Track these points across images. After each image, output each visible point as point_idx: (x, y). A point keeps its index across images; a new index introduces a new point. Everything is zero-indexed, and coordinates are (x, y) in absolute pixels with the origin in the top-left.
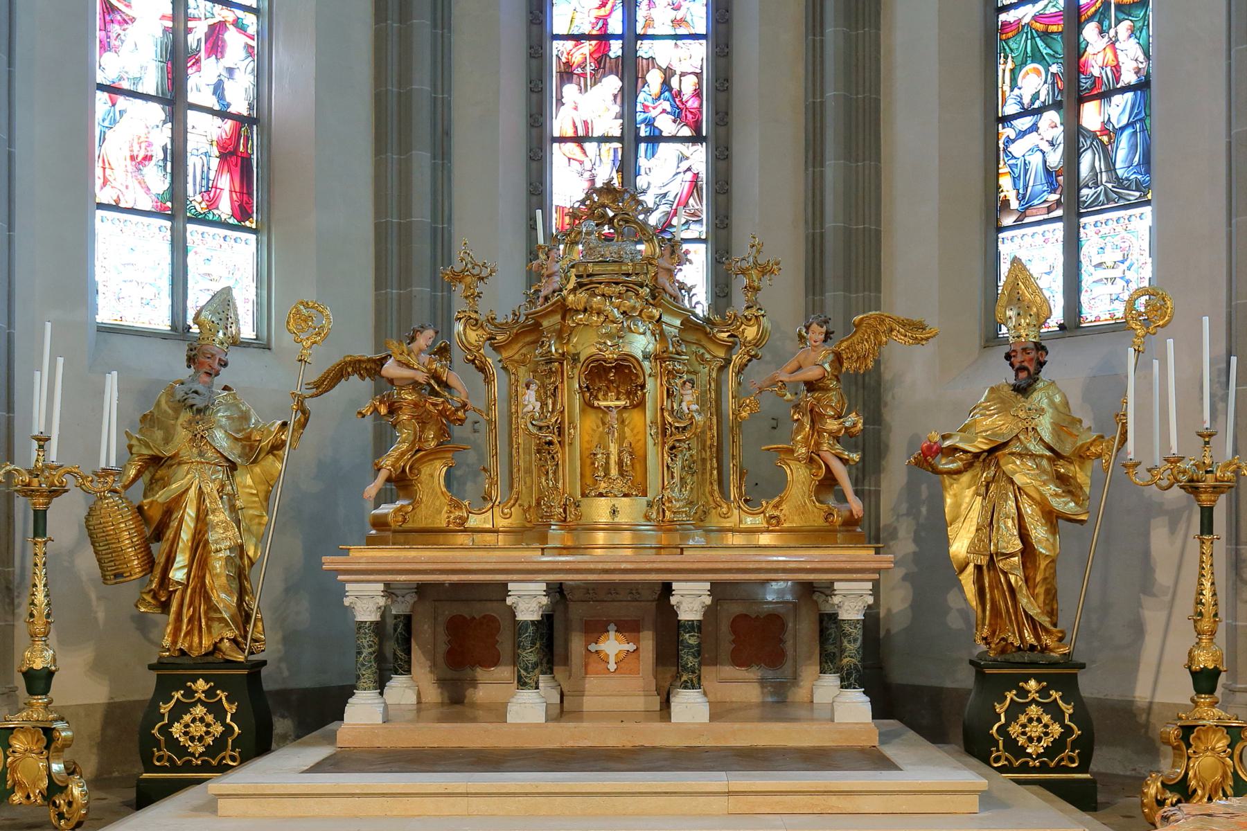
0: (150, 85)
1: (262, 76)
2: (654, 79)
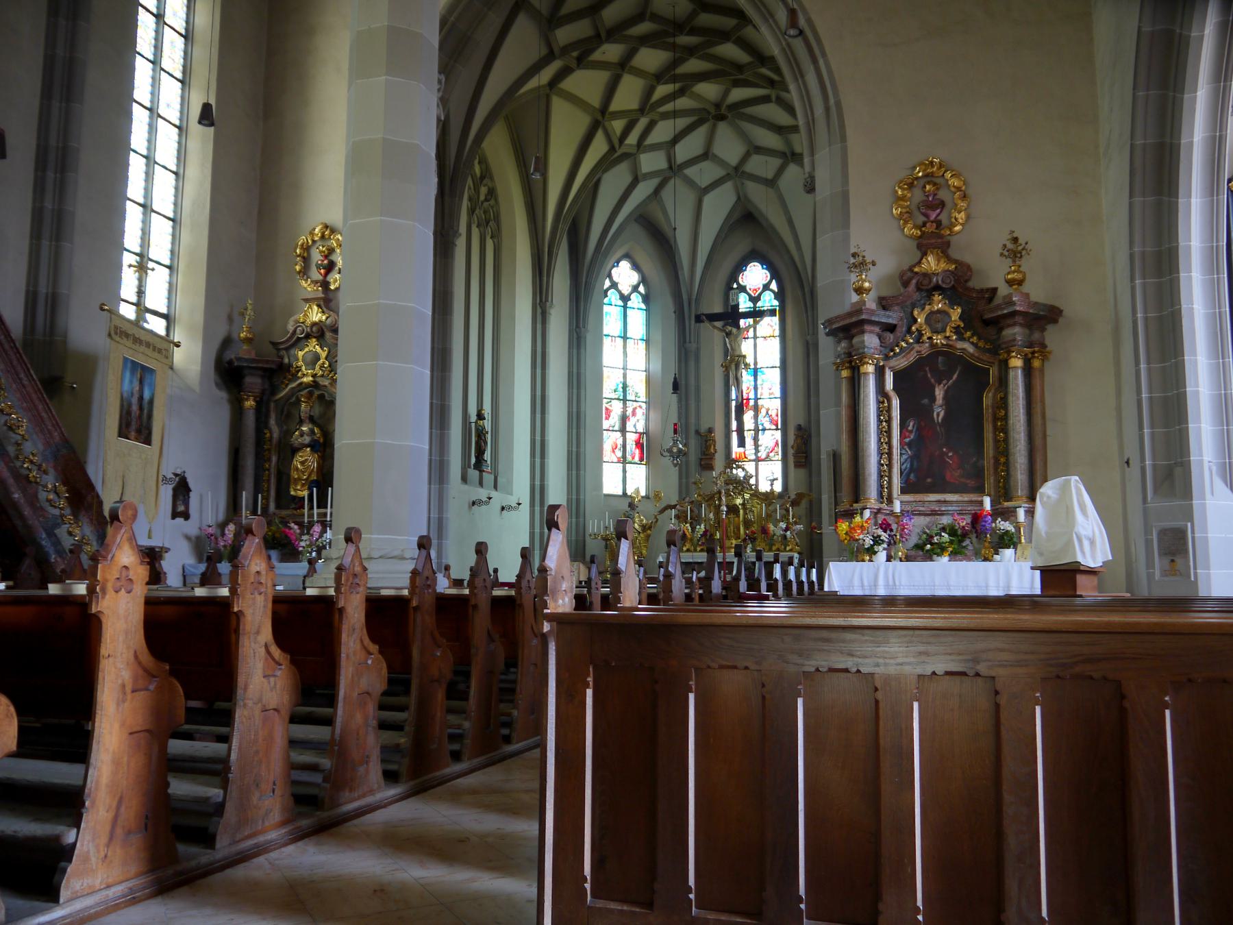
0: (617, 428)
1: (647, 420)
2: (763, 412)
